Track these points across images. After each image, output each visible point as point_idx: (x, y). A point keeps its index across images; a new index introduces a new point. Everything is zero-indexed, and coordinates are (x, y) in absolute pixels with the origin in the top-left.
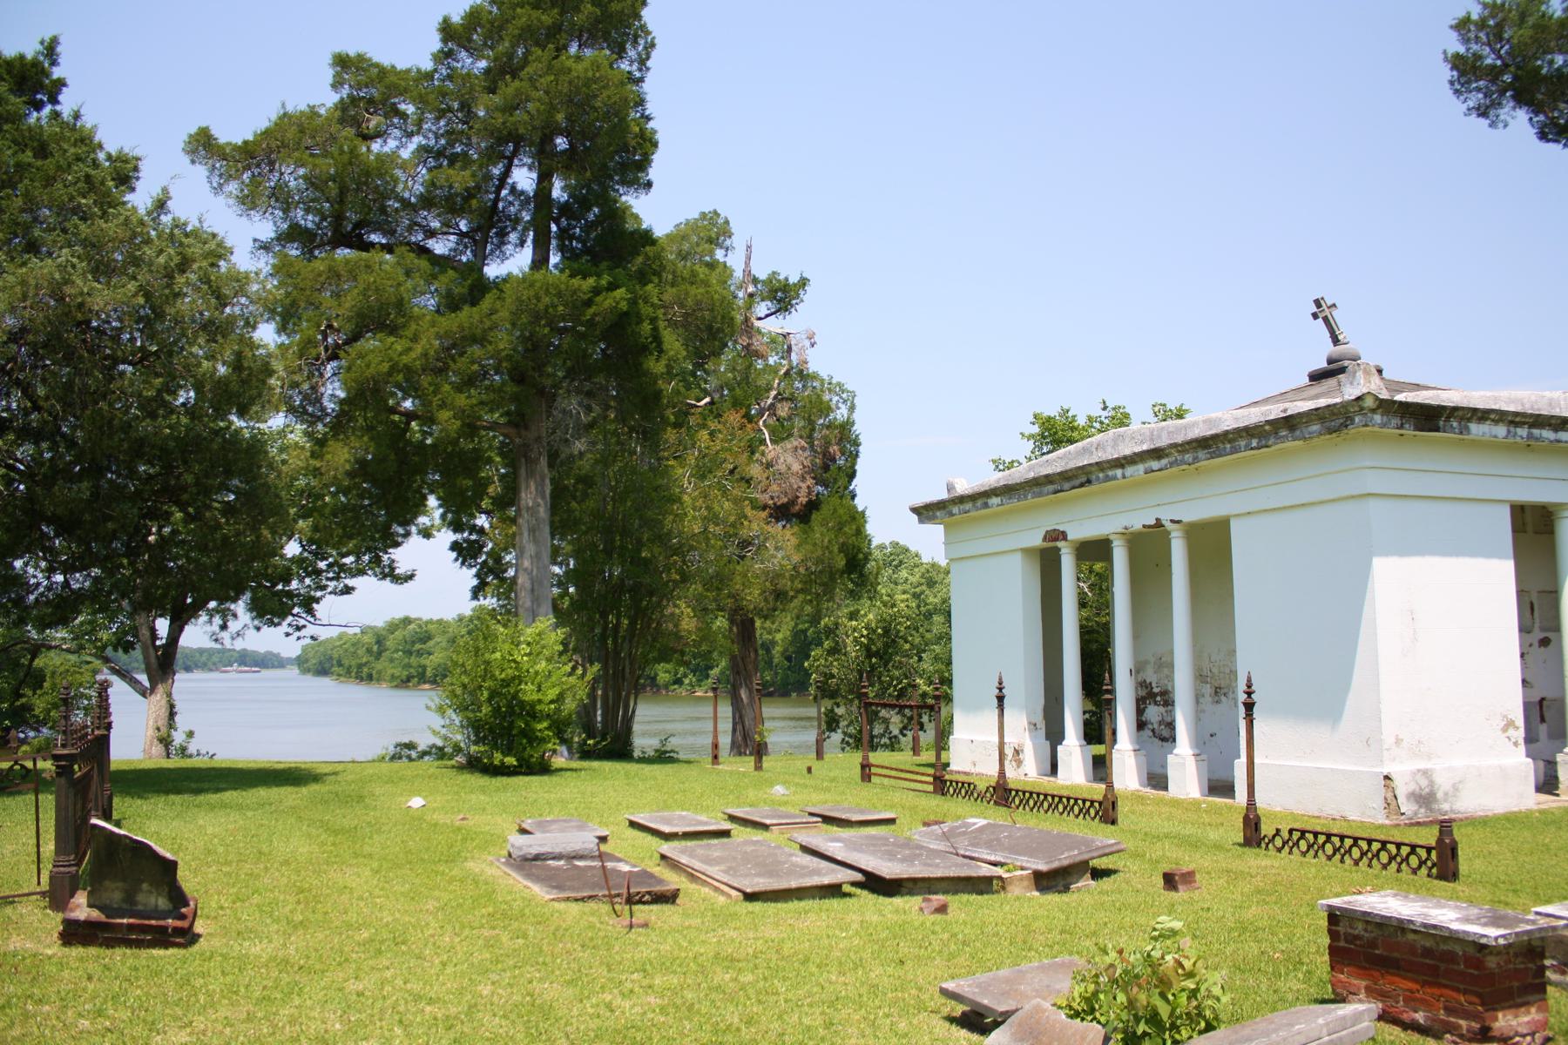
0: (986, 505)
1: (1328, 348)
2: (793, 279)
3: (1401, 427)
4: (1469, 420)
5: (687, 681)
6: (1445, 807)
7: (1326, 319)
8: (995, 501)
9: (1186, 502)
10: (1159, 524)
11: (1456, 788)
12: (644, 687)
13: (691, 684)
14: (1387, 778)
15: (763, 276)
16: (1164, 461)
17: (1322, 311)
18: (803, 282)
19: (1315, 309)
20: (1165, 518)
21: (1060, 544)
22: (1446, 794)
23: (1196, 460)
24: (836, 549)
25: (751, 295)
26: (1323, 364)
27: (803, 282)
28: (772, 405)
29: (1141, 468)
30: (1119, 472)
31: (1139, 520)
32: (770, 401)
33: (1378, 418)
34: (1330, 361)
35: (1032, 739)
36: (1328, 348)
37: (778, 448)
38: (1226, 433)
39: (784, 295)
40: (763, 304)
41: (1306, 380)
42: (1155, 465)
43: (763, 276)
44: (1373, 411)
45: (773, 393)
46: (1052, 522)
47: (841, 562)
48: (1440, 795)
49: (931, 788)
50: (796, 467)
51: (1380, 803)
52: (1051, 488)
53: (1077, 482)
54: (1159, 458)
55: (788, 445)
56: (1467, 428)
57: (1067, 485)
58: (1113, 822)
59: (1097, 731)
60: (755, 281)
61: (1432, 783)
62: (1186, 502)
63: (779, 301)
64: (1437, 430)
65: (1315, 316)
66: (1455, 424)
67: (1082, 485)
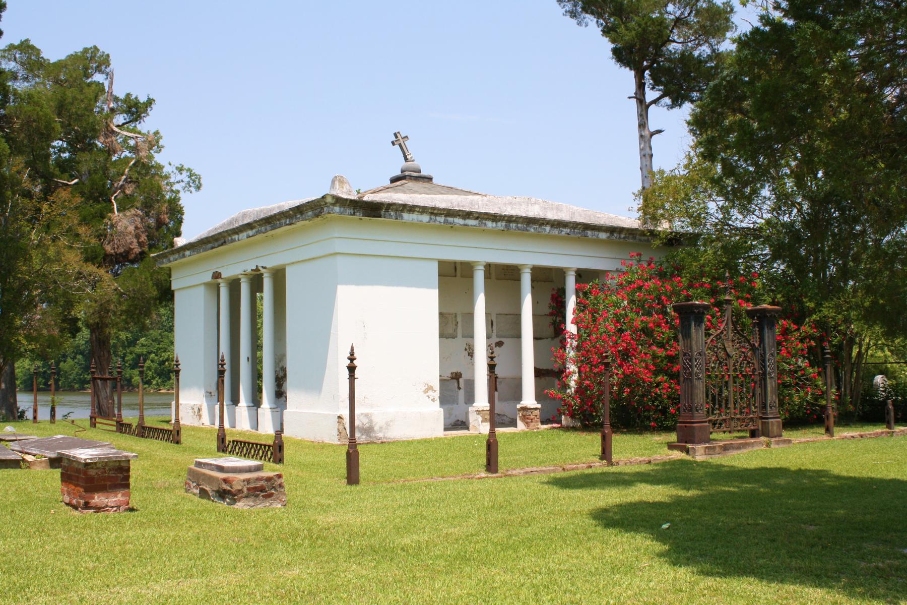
0: (184, 256)
1: (402, 163)
2: (143, 99)
3: (354, 214)
4: (402, 211)
5: (154, 382)
6: (380, 435)
7: (400, 145)
8: (187, 253)
9: (266, 257)
10: (257, 269)
11: (388, 424)
12: (122, 387)
13: (157, 384)
14: (339, 417)
15: (122, 96)
16: (254, 231)
17: (399, 141)
18: (150, 102)
19: (394, 139)
20: (260, 265)
21: (219, 280)
22: (381, 428)
23: (266, 231)
24: (150, 283)
25: (112, 110)
26: (399, 173)
27: (150, 102)
28: (122, 185)
29: (244, 234)
30: (236, 237)
31: (250, 266)
32: (121, 183)
33: (337, 209)
34: (402, 172)
35: (207, 401)
36: (402, 163)
37: (121, 214)
38: (275, 215)
39: (136, 109)
40: (122, 116)
41: (387, 183)
42: (250, 233)
43: (122, 96)
44: (334, 205)
45: (124, 177)
46: (214, 267)
47: (155, 293)
48: (376, 428)
49: (114, 428)
50: (131, 228)
51: (336, 432)
52: (210, 245)
53: (220, 242)
54: (252, 229)
55: (128, 213)
56: (402, 217)
57: (216, 244)
58: (178, 442)
59: (256, 402)
60: (116, 99)
61: (371, 421)
62: (266, 257)
63: (132, 114)
64: (380, 216)
65: (393, 143)
66: (392, 213)
67: (222, 245)
